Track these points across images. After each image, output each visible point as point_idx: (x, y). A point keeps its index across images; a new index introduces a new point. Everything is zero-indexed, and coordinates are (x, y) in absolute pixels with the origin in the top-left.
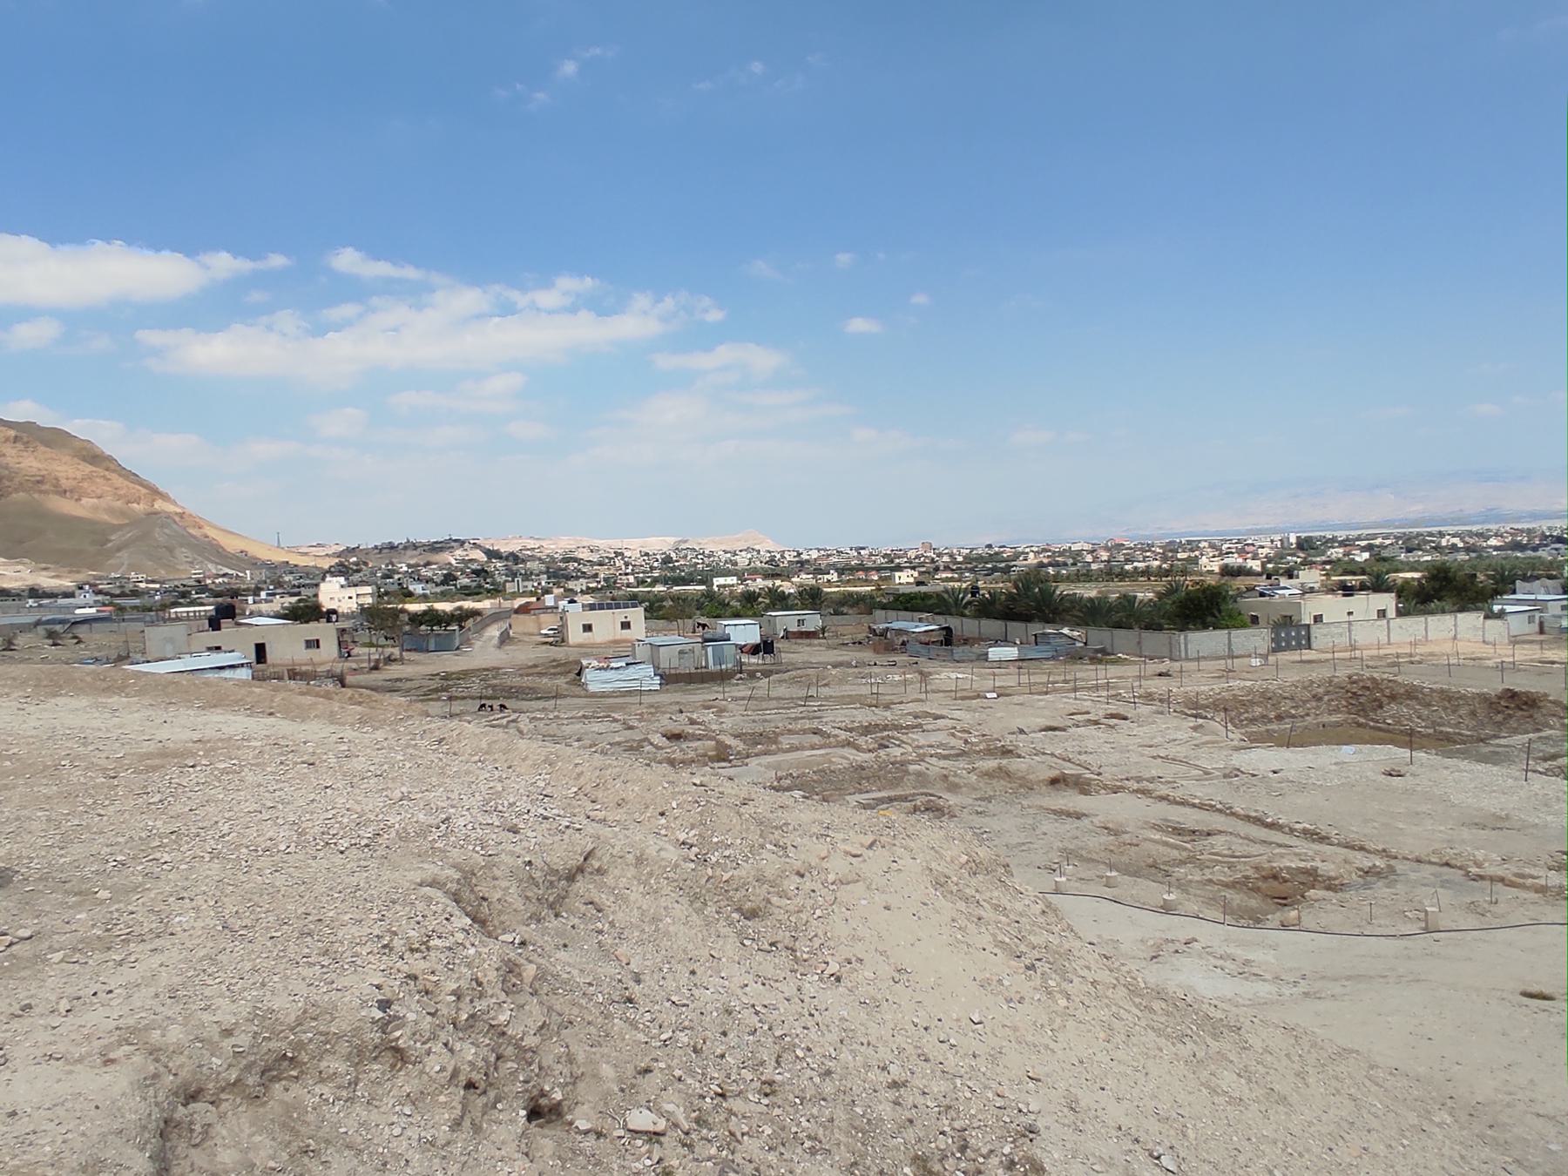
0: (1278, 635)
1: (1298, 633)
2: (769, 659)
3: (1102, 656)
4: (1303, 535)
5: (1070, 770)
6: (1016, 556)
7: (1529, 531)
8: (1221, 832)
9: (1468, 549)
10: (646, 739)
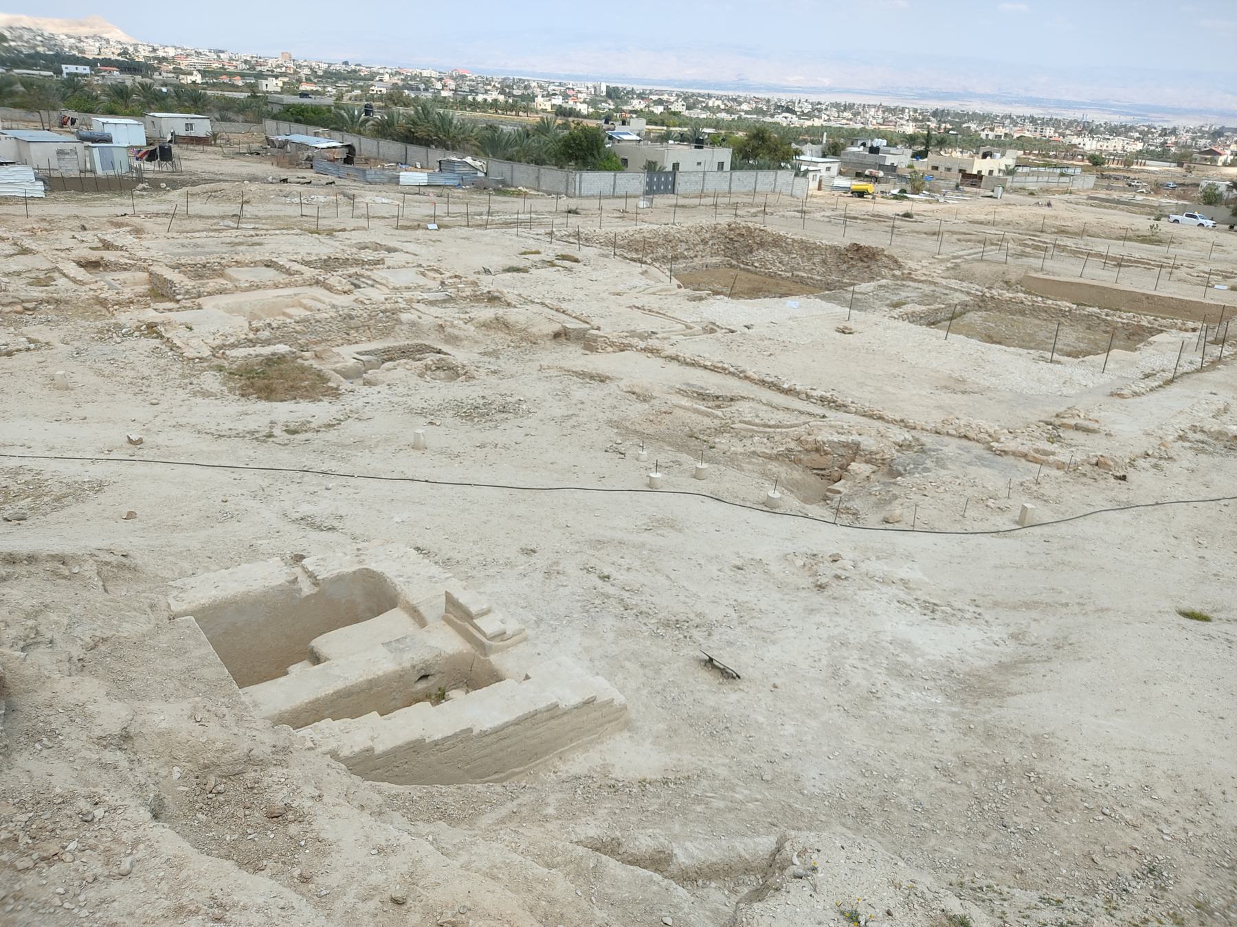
0: (651, 179)
1: (659, 179)
2: (167, 166)
3: (503, 188)
4: (612, 85)
5: (572, 325)
6: (372, 76)
7: (768, 101)
8: (743, 398)
9: (728, 111)
10: (56, 269)
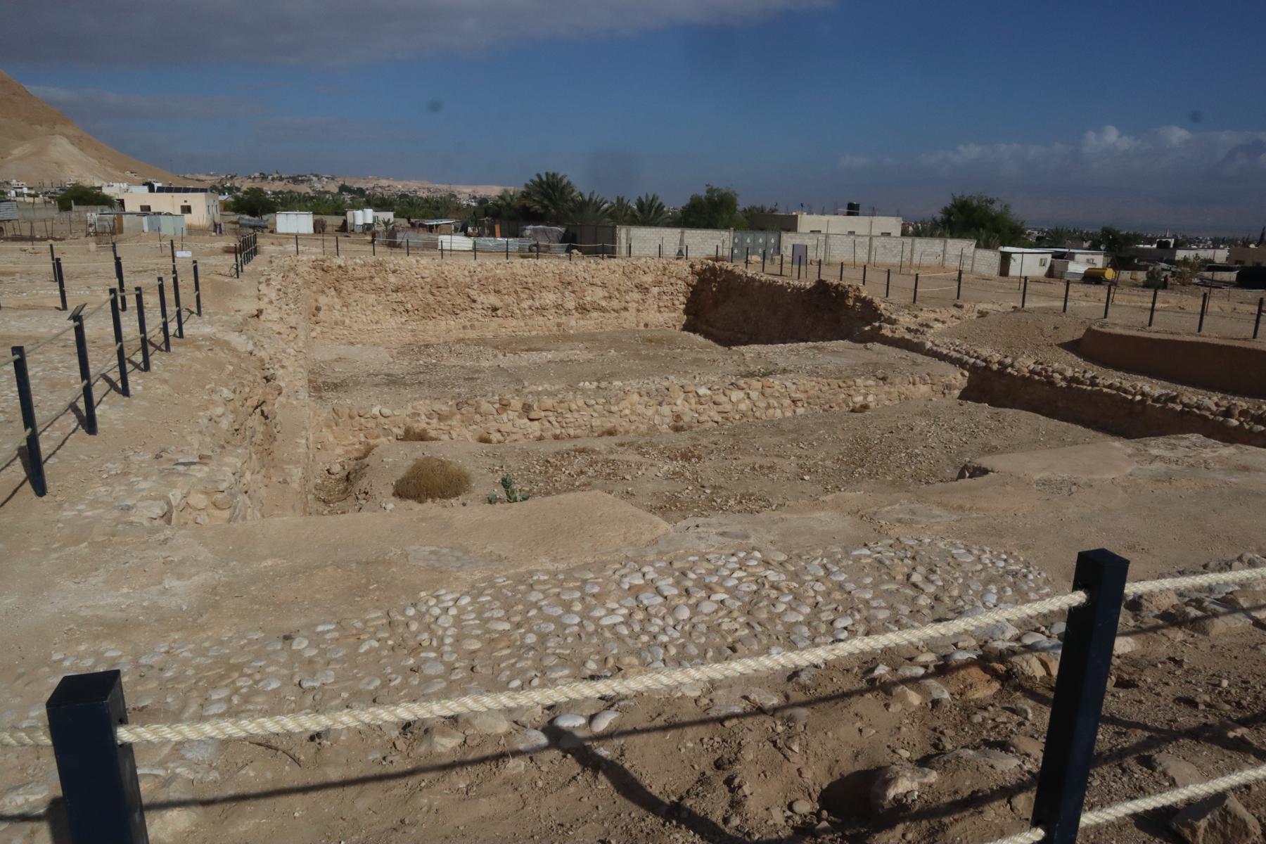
0: (742, 240)
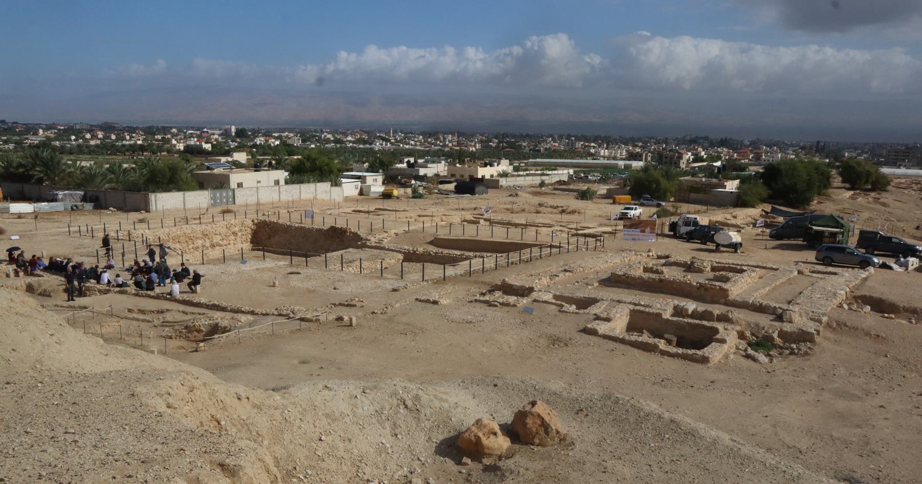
0: (215, 195)
1: (227, 194)
